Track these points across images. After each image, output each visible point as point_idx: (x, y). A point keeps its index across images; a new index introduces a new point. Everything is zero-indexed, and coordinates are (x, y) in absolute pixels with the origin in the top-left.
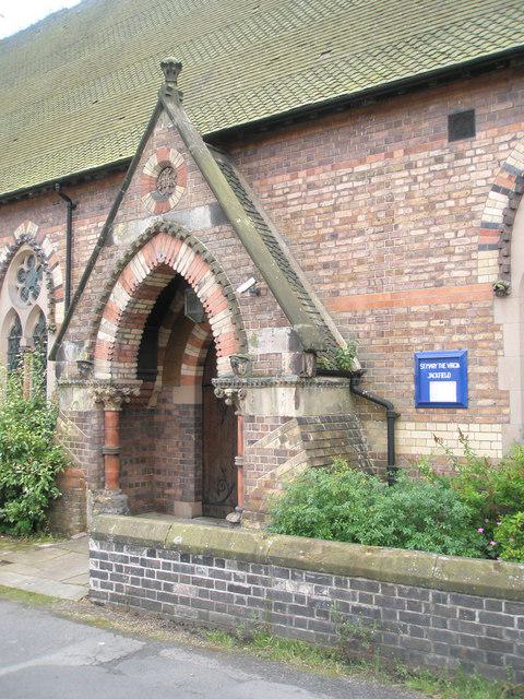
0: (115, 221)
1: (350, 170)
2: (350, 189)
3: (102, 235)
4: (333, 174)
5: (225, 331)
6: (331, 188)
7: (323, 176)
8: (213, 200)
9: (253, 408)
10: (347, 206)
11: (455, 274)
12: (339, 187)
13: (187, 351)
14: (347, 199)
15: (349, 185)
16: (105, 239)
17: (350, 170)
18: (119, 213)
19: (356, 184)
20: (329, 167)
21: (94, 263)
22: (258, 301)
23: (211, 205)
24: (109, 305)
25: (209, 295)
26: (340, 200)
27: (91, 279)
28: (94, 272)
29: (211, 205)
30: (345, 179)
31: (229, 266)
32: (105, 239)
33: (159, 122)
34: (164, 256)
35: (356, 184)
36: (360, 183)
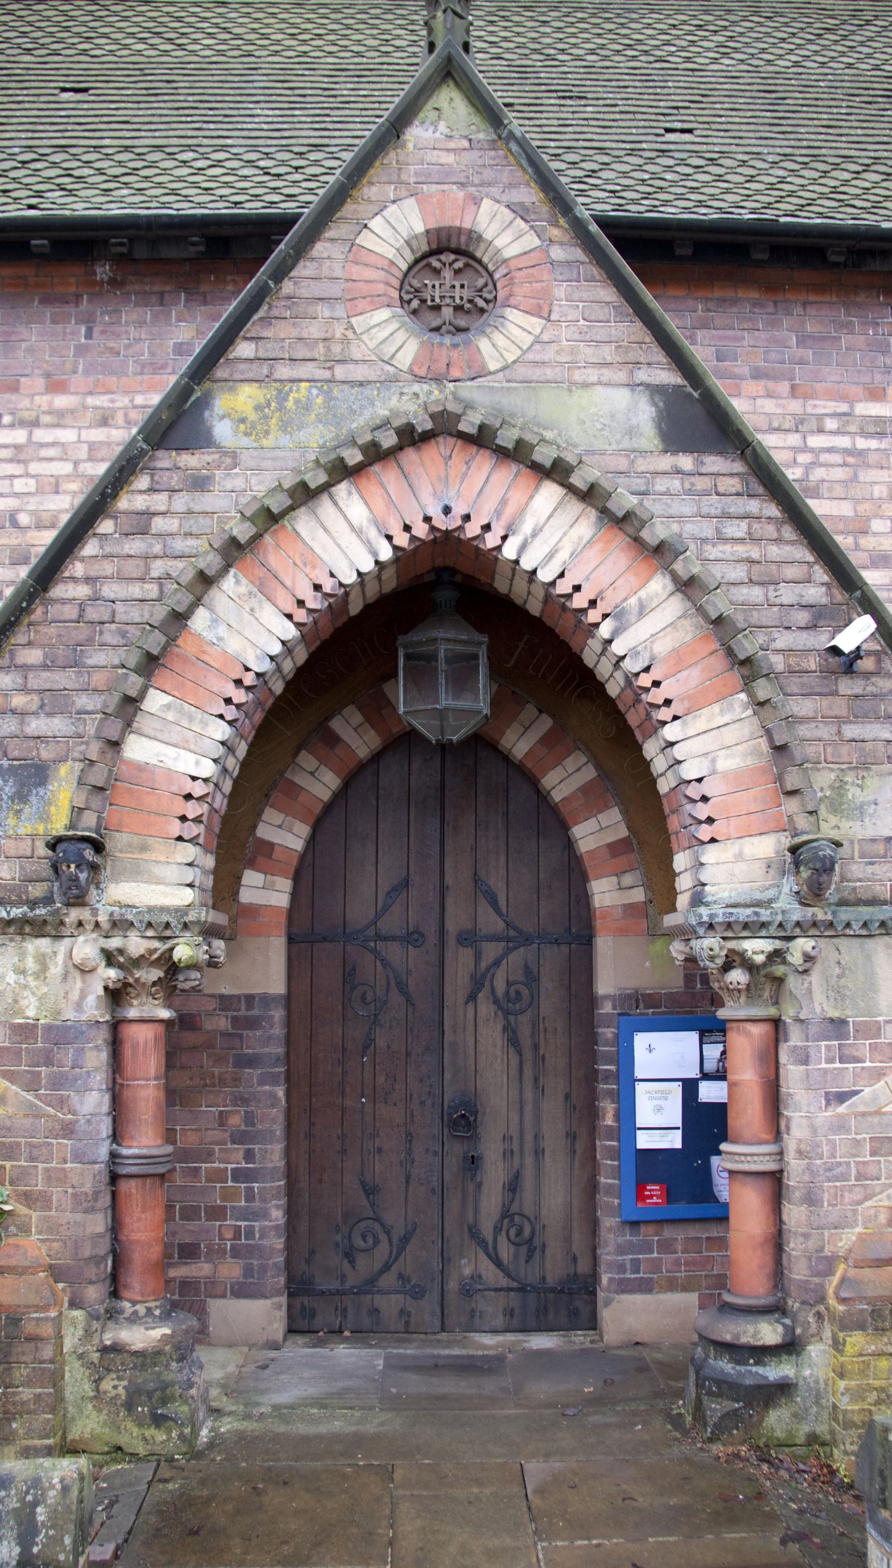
0: (221, 372)
1: (844, 408)
2: (846, 452)
3: (165, 404)
4: (795, 406)
5: (727, 763)
6: (794, 439)
7: (769, 406)
8: (669, 377)
9: (838, 994)
10: (839, 491)
11: (36, 725)
12: (815, 441)
13: (264, 832)
14: (839, 474)
15: (844, 442)
16: (171, 426)
17: (844, 408)
18: (244, 349)
19: (862, 443)
20: (784, 387)
21: (115, 496)
22: (847, 686)
23: (655, 390)
24: (185, 645)
25: (662, 647)
26: (819, 473)
27: (90, 548)
28: (106, 526)
29: (655, 390)
30: (831, 424)
31: (739, 573)
32: (171, 426)
33: (427, 112)
34: (459, 510)
35: (862, 443)
36: (873, 444)
